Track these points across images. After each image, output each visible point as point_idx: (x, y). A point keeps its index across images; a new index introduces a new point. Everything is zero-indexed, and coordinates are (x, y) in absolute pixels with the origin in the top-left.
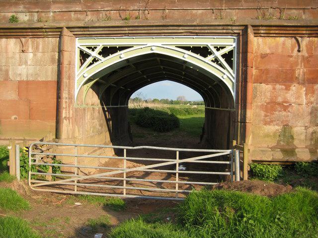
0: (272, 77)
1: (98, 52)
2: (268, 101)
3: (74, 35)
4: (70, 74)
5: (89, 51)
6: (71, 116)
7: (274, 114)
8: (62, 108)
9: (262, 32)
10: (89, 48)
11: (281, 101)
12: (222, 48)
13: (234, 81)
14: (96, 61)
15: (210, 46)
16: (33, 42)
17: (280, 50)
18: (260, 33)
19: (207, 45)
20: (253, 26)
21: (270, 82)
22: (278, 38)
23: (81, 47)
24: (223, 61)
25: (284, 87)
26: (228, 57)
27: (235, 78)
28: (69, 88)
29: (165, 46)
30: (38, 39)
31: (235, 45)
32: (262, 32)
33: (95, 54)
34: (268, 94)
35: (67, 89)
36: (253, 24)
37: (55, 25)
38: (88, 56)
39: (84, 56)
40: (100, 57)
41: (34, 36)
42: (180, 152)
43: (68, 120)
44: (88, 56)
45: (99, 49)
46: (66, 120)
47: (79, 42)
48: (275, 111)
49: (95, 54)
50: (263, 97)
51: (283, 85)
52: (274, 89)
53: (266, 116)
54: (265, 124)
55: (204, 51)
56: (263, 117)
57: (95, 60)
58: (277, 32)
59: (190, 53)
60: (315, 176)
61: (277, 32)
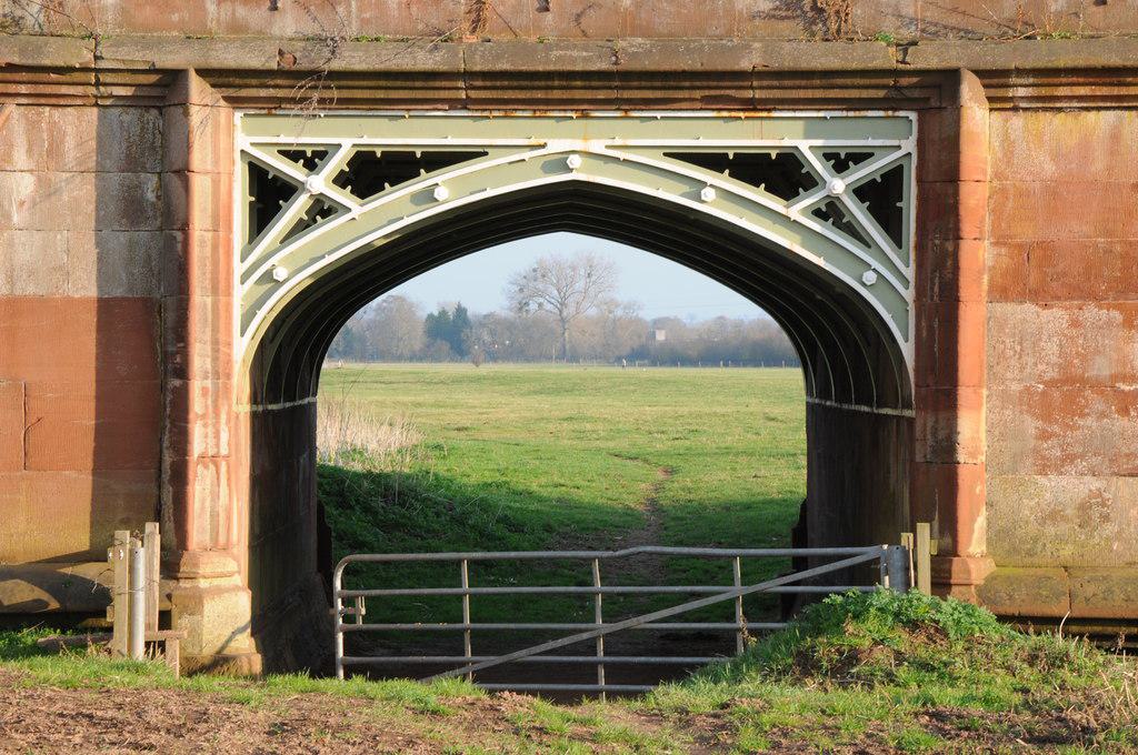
0: (1065, 274)
2: (1052, 374)
3: (225, 98)
5: (294, 171)
6: (224, 451)
7: (1073, 428)
8: (191, 416)
9: (1021, 92)
10: (294, 155)
11: (1106, 372)
12: (859, 157)
13: (909, 294)
16: (33, 126)
17: (1098, 165)
18: (1011, 99)
19: (796, 148)
20: (980, 73)
21: (1058, 298)
22: (1092, 115)
24: (858, 212)
25: (1117, 316)
26: (881, 196)
27: (912, 284)
28: (215, 330)
29: (621, 155)
30: (57, 113)
31: (909, 145)
32: (1021, 92)
33: (320, 183)
34: (1051, 349)
35: (208, 336)
36: (982, 66)
37: (138, 56)
38: (287, 190)
39: (269, 194)
40: (343, 196)
41: (38, 100)
42: (745, 560)
43: (211, 466)
44: (287, 190)
45: (337, 163)
46: (206, 467)
47: (249, 133)
48: (1082, 415)
49: (320, 183)
50: (1031, 360)
51: (1118, 307)
52: (1075, 324)
53: (1044, 436)
54: (1043, 471)
55: (369, 174)
56: (1033, 443)
58: (1082, 91)
59: (724, 181)
60: (1130, 651)
61: (1082, 91)
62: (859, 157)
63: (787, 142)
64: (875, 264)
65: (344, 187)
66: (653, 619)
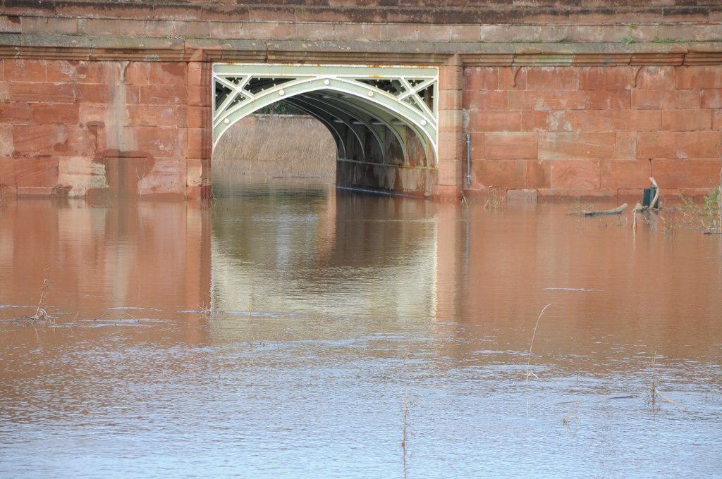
1: (405, 93)
4: (386, 177)
5: (230, 85)
10: (230, 79)
12: (419, 82)
14: (241, 100)
15: (403, 79)
23: (217, 77)
31: (437, 78)
33: (238, 89)
40: (247, 94)
45: (245, 82)
49: (238, 89)
55: (256, 85)
57: (239, 98)
62: (419, 82)
63: (396, 76)
64: (426, 118)
65: (248, 90)
66: (275, 88)
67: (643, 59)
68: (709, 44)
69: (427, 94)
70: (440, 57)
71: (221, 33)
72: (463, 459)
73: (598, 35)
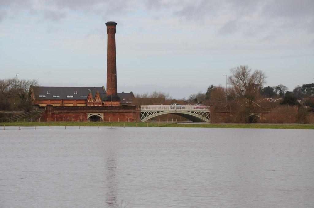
55: (90, 115)
67: (117, 113)
68: (5, 128)
69: (102, 115)
70: (103, 113)
71: (88, 111)
72: (105, 123)
73: (113, 111)
